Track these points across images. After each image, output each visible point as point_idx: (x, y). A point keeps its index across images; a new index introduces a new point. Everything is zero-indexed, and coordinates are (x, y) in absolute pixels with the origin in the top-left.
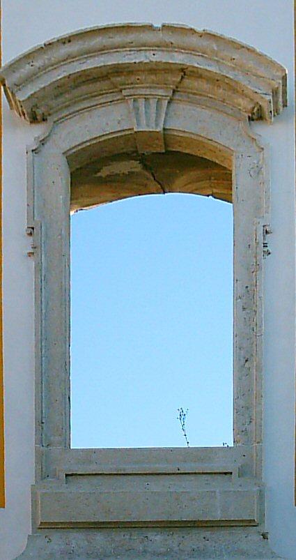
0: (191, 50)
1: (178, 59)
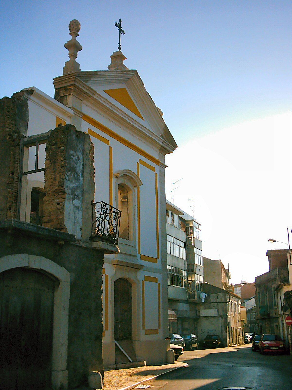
1: (132, 177)
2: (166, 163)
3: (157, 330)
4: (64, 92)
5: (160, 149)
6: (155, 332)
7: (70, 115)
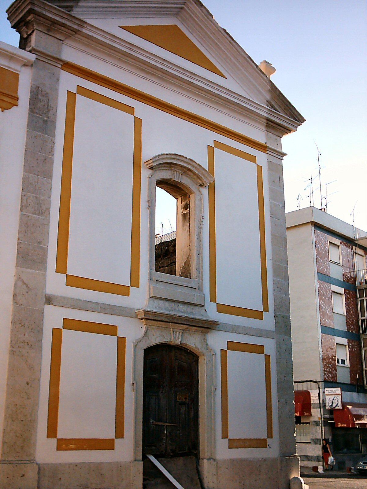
0: (193, 166)
1: (189, 167)
2: (284, 150)
3: (266, 439)
4: (27, 30)
5: (268, 126)
6: (261, 443)
7: (26, 61)
